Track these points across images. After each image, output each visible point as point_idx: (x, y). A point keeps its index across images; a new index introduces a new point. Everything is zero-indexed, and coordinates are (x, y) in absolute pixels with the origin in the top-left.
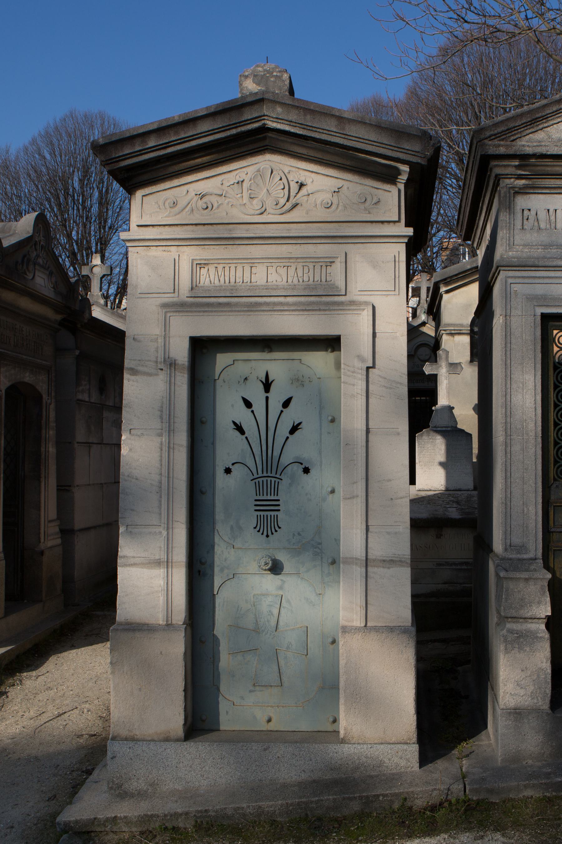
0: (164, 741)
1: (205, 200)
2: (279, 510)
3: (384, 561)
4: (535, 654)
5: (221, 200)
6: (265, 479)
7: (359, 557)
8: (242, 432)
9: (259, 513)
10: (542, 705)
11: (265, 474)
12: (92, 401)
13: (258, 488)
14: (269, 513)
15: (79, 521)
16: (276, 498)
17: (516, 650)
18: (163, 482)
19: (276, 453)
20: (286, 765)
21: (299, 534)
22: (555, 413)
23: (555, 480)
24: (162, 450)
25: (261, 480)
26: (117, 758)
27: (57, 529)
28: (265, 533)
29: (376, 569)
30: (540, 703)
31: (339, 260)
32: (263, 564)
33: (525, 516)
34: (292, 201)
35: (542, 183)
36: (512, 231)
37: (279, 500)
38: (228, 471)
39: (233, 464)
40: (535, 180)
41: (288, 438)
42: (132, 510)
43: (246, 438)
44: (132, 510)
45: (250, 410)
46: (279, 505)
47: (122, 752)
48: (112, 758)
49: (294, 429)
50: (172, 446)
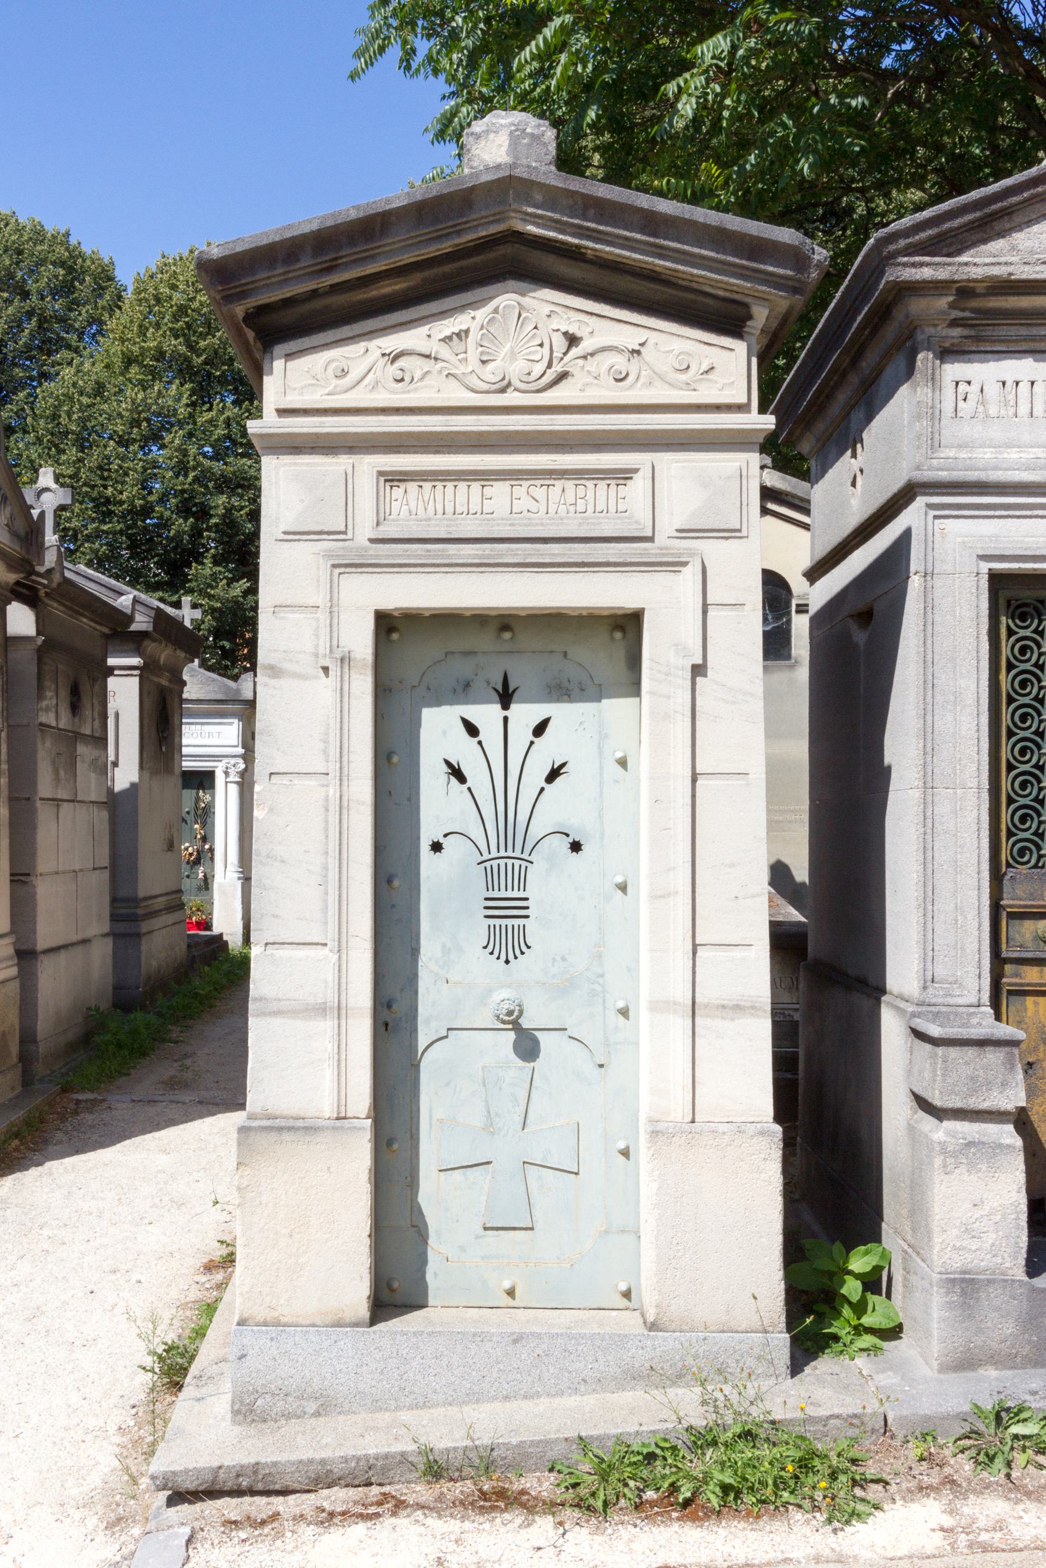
0: (333, 1326)
1: (401, 363)
2: (527, 917)
3: (724, 1007)
4: (997, 1175)
5: (427, 365)
6: (502, 862)
7: (681, 1000)
8: (461, 778)
9: (492, 922)
10: (1011, 1268)
11: (502, 853)
12: (61, 726)
13: (491, 878)
14: (510, 922)
15: (45, 935)
16: (521, 895)
17: (963, 1169)
18: (331, 866)
19: (522, 818)
20: (552, 1371)
21: (564, 959)
22: (1009, 747)
23: (1008, 865)
24: (327, 810)
25: (495, 863)
26: (248, 1358)
27: (11, 951)
28: (503, 957)
29: (709, 1020)
30: (1007, 1265)
31: (640, 474)
32: (504, 1011)
33: (959, 931)
34: (558, 368)
35: (995, 334)
36: (937, 422)
37: (526, 899)
38: (437, 847)
39: (445, 836)
40: (981, 328)
41: (542, 789)
42: (276, 916)
43: (469, 789)
44: (276, 916)
45: (477, 739)
46: (527, 908)
47: (257, 1348)
48: (240, 1358)
49: (554, 775)
50: (345, 803)
